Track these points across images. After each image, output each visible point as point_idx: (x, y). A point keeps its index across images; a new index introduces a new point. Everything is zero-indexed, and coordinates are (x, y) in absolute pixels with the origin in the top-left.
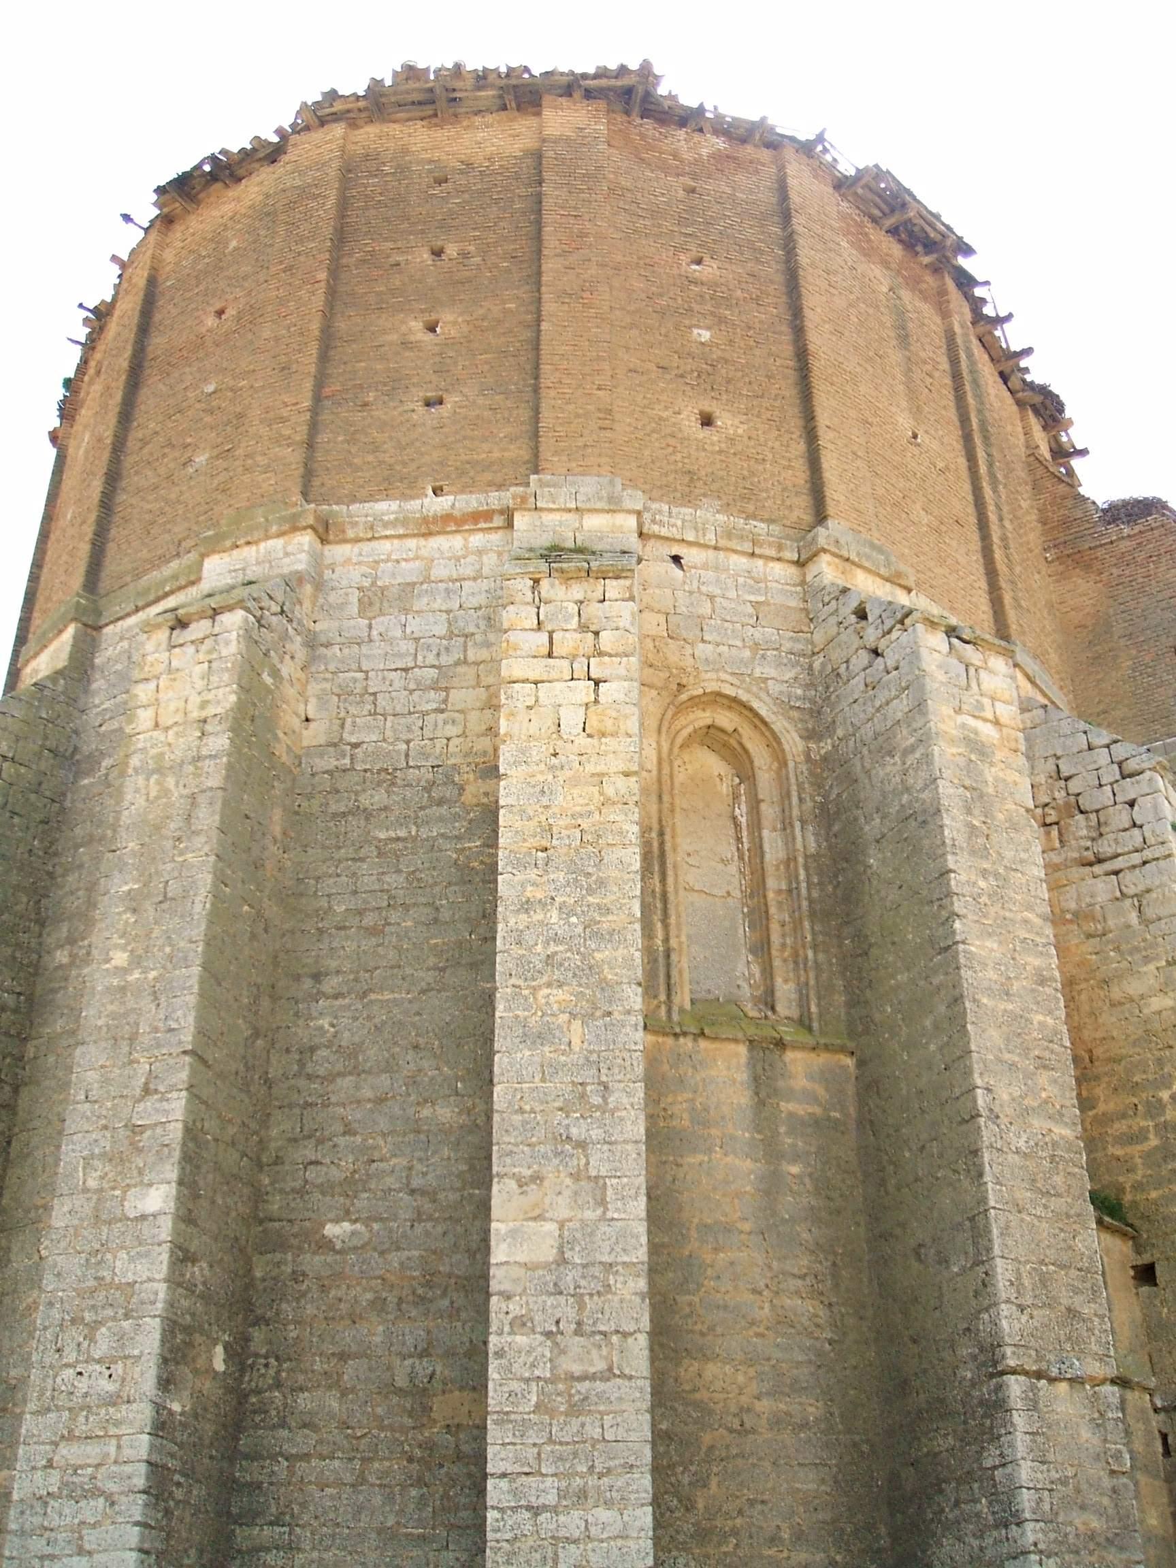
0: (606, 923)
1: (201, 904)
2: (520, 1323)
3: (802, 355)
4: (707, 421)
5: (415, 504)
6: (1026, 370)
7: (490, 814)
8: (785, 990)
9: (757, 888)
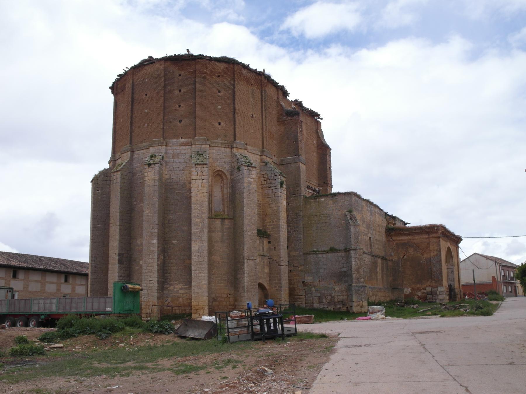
0: (204, 211)
1: (157, 205)
2: (195, 256)
3: (234, 109)
4: (219, 123)
5: (179, 140)
7: (190, 190)
8: (226, 210)
9: (223, 196)
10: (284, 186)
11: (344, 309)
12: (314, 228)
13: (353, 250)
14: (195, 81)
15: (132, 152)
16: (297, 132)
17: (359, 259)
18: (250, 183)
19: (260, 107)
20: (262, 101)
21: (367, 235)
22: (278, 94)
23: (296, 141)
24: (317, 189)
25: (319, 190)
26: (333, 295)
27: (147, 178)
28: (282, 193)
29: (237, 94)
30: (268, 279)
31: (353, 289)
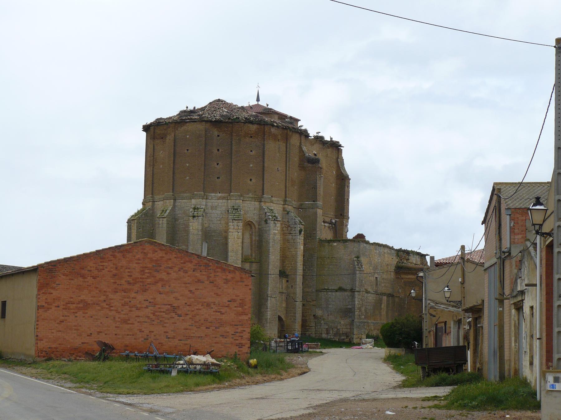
3: (264, 166)
4: (251, 180)
5: (216, 195)
6: (301, 126)
8: (253, 255)
10: (303, 232)
11: (347, 340)
12: (327, 269)
13: (357, 291)
14: (231, 142)
15: (175, 200)
16: (317, 180)
17: (361, 300)
18: (275, 234)
19: (285, 160)
20: (286, 153)
21: (373, 276)
22: (301, 140)
23: (315, 188)
24: (334, 221)
25: (335, 222)
26: (339, 328)
27: (191, 227)
28: (300, 239)
29: (266, 153)
30: (285, 312)
31: (355, 324)
